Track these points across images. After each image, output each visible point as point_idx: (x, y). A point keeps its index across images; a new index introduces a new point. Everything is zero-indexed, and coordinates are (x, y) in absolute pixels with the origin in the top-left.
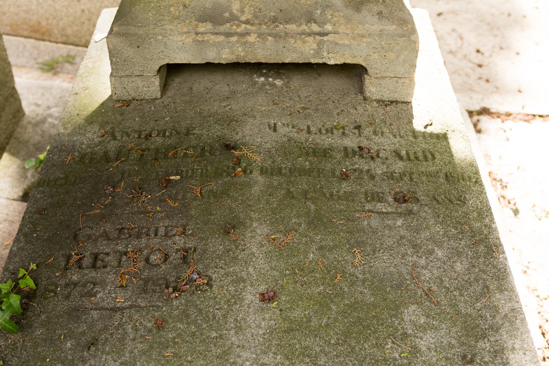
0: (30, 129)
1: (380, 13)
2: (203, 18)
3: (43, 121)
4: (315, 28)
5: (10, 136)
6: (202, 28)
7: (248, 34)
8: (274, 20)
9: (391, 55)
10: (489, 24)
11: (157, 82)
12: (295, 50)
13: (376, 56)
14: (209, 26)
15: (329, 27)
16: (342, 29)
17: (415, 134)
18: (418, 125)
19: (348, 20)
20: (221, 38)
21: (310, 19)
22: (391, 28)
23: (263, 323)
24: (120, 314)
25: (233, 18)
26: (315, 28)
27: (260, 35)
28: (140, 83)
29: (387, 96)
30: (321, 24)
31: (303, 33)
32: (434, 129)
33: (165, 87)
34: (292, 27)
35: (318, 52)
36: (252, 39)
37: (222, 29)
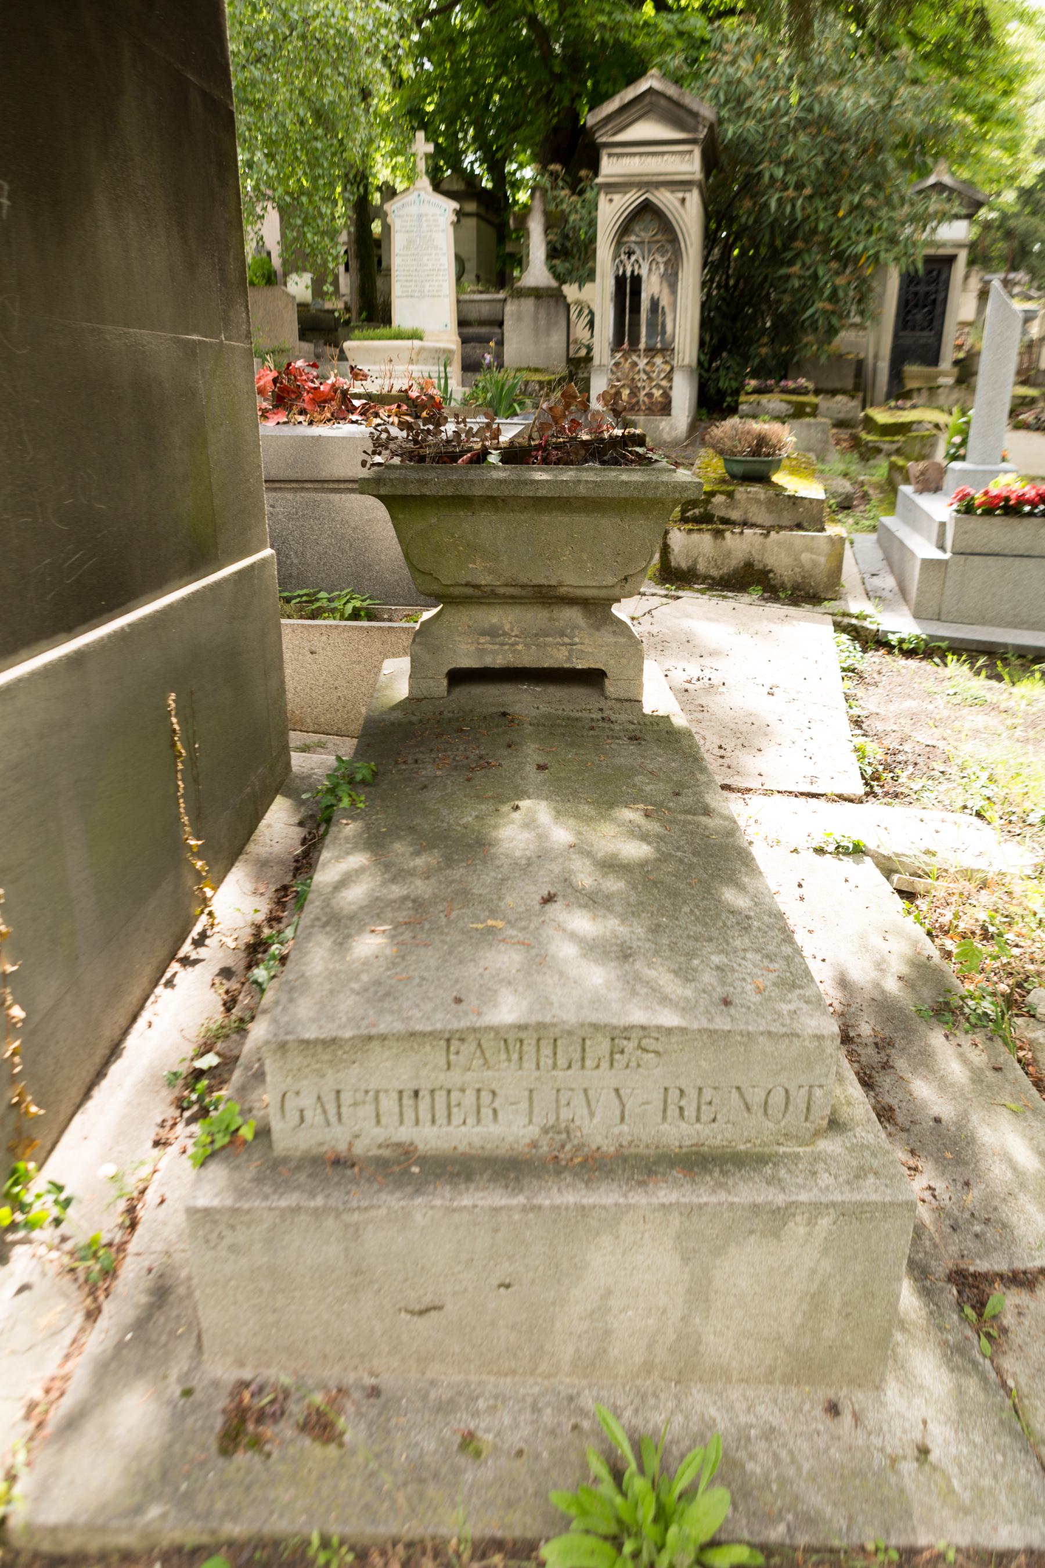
0: (298, 781)
1: (614, 632)
2: (483, 633)
3: (310, 776)
4: (567, 640)
5: (282, 783)
6: (482, 640)
7: (517, 644)
8: (536, 635)
9: (624, 661)
10: (1033, 1016)
11: (445, 682)
12: (552, 657)
13: (612, 662)
14: (488, 638)
15: (577, 640)
16: (586, 641)
17: (644, 715)
18: (647, 710)
19: (591, 635)
20: (497, 647)
21: (563, 634)
22: (623, 640)
23: (528, 1233)
24: (673, 58)
25: (505, 634)
26: (567, 640)
27: (526, 645)
28: (432, 683)
29: (623, 695)
30: (571, 638)
31: (558, 644)
32: (661, 713)
33: (449, 692)
34: (550, 639)
35: (569, 659)
36: (520, 647)
37: (498, 640)
